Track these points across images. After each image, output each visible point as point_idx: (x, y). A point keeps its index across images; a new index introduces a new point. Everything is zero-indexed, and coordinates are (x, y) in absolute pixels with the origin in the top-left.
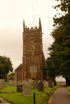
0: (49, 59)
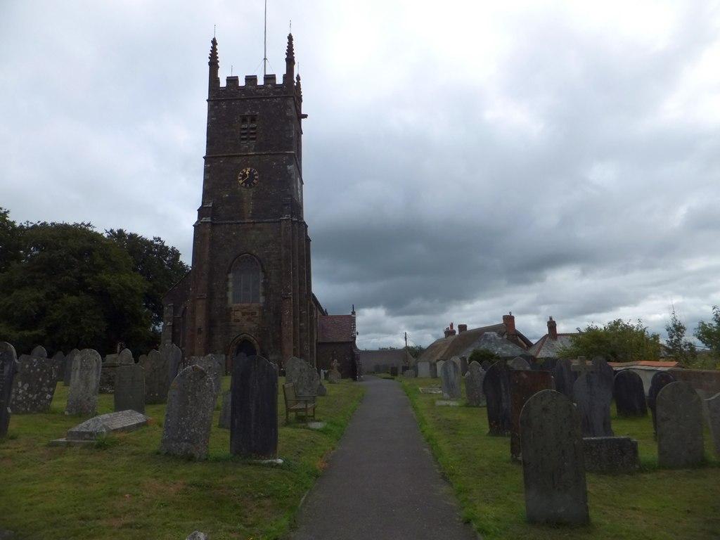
0: (287, 168)
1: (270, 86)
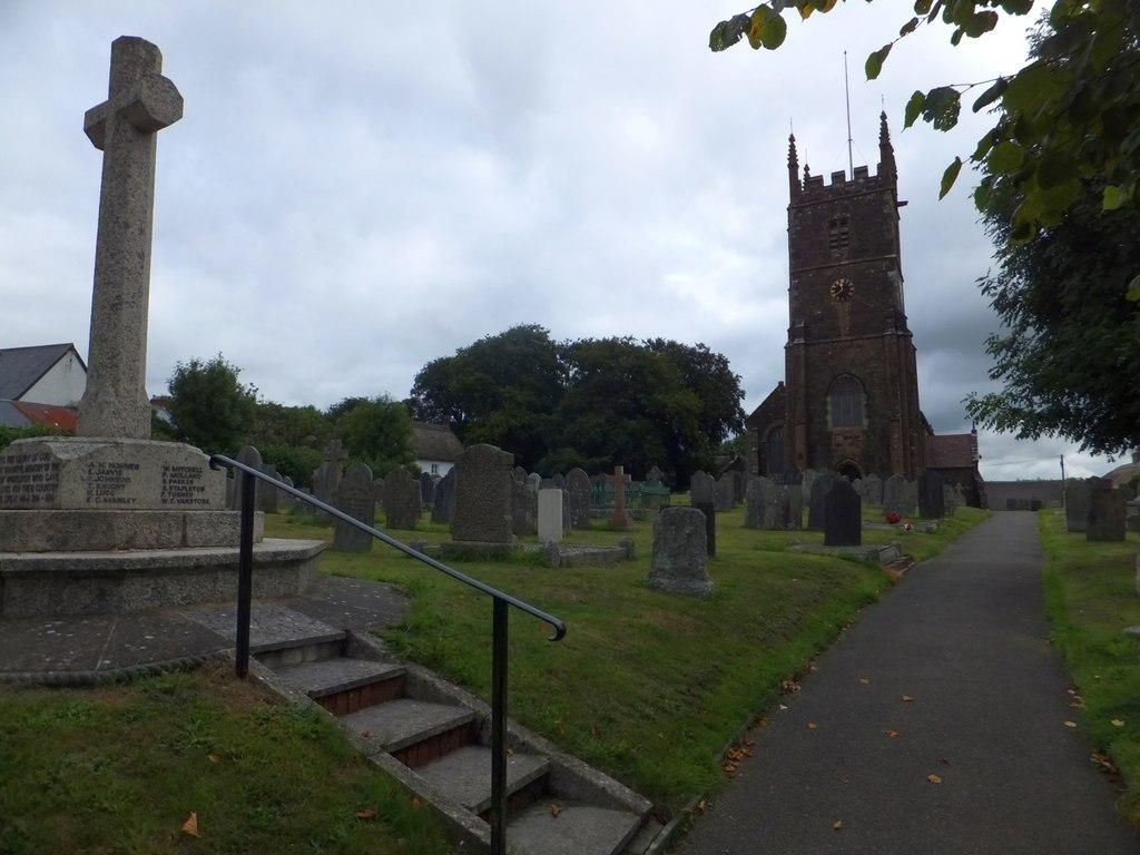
1: (861, 180)
